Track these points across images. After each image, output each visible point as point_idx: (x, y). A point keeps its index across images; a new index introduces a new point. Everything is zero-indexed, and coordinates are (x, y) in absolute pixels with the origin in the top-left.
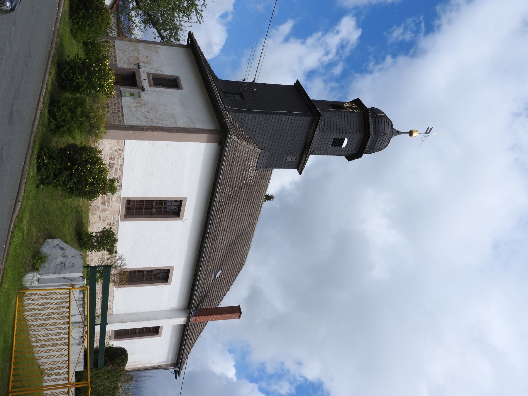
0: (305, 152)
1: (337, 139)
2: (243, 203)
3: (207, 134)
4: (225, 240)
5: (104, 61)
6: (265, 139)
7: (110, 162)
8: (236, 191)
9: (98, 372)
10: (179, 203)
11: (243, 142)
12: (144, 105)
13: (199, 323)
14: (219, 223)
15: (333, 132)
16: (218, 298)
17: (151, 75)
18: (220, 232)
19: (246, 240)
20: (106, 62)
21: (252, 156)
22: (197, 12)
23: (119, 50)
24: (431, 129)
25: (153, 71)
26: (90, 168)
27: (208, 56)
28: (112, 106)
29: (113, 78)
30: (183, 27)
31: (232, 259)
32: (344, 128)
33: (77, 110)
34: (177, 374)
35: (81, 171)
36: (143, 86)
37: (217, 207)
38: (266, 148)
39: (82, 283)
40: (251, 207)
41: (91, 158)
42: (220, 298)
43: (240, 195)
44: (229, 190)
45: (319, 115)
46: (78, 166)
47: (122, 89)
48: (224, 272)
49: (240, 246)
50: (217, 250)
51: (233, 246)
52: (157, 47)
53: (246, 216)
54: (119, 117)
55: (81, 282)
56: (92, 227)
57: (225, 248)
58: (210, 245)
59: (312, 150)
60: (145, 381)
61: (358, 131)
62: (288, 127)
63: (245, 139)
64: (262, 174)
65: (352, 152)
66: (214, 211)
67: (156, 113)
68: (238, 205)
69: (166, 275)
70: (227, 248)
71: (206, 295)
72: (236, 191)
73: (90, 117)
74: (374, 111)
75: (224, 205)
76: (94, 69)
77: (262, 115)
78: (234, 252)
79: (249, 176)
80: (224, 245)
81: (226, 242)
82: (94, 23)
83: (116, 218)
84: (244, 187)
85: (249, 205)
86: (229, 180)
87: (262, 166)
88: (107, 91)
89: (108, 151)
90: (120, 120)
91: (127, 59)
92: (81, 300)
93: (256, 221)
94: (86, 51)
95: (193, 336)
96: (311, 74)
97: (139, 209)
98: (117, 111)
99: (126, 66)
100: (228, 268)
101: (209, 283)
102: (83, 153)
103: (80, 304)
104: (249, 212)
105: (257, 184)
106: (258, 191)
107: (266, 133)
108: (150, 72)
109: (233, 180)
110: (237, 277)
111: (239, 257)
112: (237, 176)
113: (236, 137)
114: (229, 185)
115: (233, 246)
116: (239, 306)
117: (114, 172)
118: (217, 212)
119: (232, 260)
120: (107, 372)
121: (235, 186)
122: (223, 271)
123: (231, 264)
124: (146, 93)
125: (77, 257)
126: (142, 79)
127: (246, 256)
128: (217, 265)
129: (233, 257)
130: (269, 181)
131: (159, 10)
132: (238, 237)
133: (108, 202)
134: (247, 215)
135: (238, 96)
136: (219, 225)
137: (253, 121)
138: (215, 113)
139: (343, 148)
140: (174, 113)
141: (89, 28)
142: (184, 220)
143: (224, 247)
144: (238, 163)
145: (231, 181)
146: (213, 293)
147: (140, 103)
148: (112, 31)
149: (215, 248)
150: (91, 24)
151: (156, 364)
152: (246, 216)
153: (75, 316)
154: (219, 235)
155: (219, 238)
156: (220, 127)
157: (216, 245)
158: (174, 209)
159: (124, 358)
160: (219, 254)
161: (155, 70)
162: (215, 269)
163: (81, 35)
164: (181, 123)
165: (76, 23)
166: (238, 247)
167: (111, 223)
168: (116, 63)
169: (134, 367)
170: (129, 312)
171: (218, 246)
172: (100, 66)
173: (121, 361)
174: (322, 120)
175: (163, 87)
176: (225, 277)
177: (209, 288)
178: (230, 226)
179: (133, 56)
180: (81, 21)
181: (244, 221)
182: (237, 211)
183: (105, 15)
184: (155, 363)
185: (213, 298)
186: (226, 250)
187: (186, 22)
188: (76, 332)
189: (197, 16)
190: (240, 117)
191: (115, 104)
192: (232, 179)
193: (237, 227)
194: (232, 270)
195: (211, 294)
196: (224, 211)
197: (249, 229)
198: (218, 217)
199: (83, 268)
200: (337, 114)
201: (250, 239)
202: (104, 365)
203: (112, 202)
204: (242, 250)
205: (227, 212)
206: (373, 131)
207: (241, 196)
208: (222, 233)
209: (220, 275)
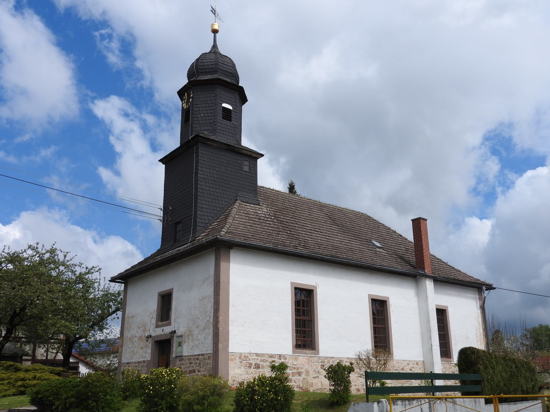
0: (239, 151)
1: (223, 115)
2: (297, 218)
3: (220, 263)
4: (338, 238)
5: (142, 380)
6: (225, 196)
7: (254, 368)
8: (283, 227)
9: (486, 379)
10: (297, 291)
11: (228, 221)
12: (190, 331)
13: (432, 264)
14: (319, 245)
15: (216, 120)
16: (403, 243)
17: (157, 323)
18: (329, 244)
19: (338, 213)
20: (143, 378)
21: (243, 210)
22: (88, 273)
23: (132, 359)
24: (212, 8)
25: (154, 321)
26: (258, 396)
27: (138, 258)
28: (193, 367)
29: (160, 369)
30: (106, 287)
31: (360, 229)
32: (211, 108)
33: (196, 410)
34: (490, 287)
35: (262, 405)
36: (170, 333)
37: (301, 248)
38: (234, 195)
39: (385, 404)
40: (301, 209)
41: (248, 394)
42: (404, 240)
43: (288, 222)
44: (282, 235)
45: (197, 136)
46: (257, 409)
47: (174, 356)
48: (374, 238)
49: (345, 220)
50: (350, 247)
51: (345, 228)
52: (128, 316)
53: (311, 214)
54: (204, 359)
55: (384, 404)
56: (326, 386)
57: (347, 238)
58: (344, 255)
59: (235, 142)
60: (498, 322)
61: (214, 93)
62: (211, 171)
63: (225, 219)
64: (264, 198)
65: (238, 98)
66: (306, 251)
67: (199, 318)
68: (298, 225)
69: (378, 302)
70: (347, 235)
71: (401, 258)
72: (283, 227)
73: (203, 395)
74: (191, 73)
75: (299, 240)
76: (151, 390)
77: (198, 201)
78: (352, 226)
79: (266, 213)
80: (344, 238)
81: (340, 236)
82: (102, 390)
83: (316, 359)
84: (279, 218)
85: (298, 211)
86: (271, 235)
87: (254, 199)
88: (175, 376)
89: (242, 370)
90: (207, 358)
91: (142, 350)
92: (404, 404)
93: (316, 203)
94: (134, 397)
95: (446, 270)
96: (154, 147)
97: (305, 334)
98: (197, 361)
99: (149, 351)
100: (370, 232)
101: (387, 255)
102: (242, 404)
103: (409, 403)
104: (307, 211)
105: (275, 203)
106: (283, 202)
107: (219, 195)
108: (155, 325)
109: (271, 231)
110: (380, 222)
111: (358, 221)
112: (266, 226)
113: (223, 230)
114: (277, 235)
115: (345, 228)
116: (412, 220)
117: (265, 363)
118: (307, 248)
119: (361, 228)
120: (486, 370)
121: (278, 228)
122: (374, 239)
123: (366, 229)
124: (177, 329)
125: (356, 409)
126: (163, 333)
127: (356, 213)
128: (367, 246)
129: (357, 227)
130: (272, 190)
131: (87, 314)
132: (335, 223)
133: (297, 369)
134: (310, 214)
135: (178, 227)
136: (322, 245)
137: (205, 210)
138: (197, 253)
139: (233, 108)
140: (199, 298)
141: (108, 396)
142: (317, 284)
143: (346, 239)
144: (251, 226)
145: (272, 233)
146: (399, 249)
147: (188, 336)
148: (113, 364)
149: (348, 249)
150: (104, 394)
151: (479, 311)
152: (311, 214)
153: (423, 409)
154: (333, 245)
155: (336, 244)
156: (212, 248)
157: (344, 248)
158: (305, 296)
159: (470, 351)
160: (354, 244)
161: (153, 319)
162: (371, 248)
163: (116, 403)
164: (209, 291)
165: (103, 409)
166: (347, 222)
167: (321, 365)
168: (146, 362)
169: (482, 336)
170: (421, 342)
171: (345, 246)
172: (148, 384)
173: (473, 355)
174: (202, 132)
175: (170, 310)
176: (380, 236)
177: (393, 254)
178: (322, 232)
179: (138, 344)
180: (101, 404)
181: (317, 216)
182: (305, 225)
183: (93, 379)
184: (478, 312)
185: (404, 249)
186: (350, 236)
187: (99, 285)
188: (441, 406)
189: (93, 273)
190: (201, 225)
191: (190, 363)
192: (270, 232)
193: (324, 224)
194: (372, 228)
195: (399, 252)
196: (306, 240)
197: (325, 210)
198: (312, 246)
199: (368, 403)
200: (195, 116)
201: (338, 209)
202: (478, 373)
203: (298, 364)
204: (349, 218)
205: (307, 236)
206: (213, 75)
207: (288, 221)
208: (331, 242)
209: (378, 242)
